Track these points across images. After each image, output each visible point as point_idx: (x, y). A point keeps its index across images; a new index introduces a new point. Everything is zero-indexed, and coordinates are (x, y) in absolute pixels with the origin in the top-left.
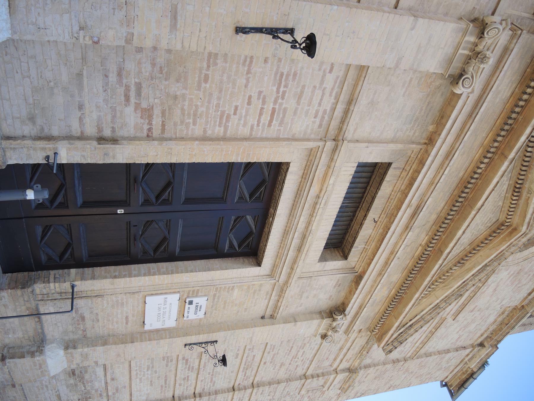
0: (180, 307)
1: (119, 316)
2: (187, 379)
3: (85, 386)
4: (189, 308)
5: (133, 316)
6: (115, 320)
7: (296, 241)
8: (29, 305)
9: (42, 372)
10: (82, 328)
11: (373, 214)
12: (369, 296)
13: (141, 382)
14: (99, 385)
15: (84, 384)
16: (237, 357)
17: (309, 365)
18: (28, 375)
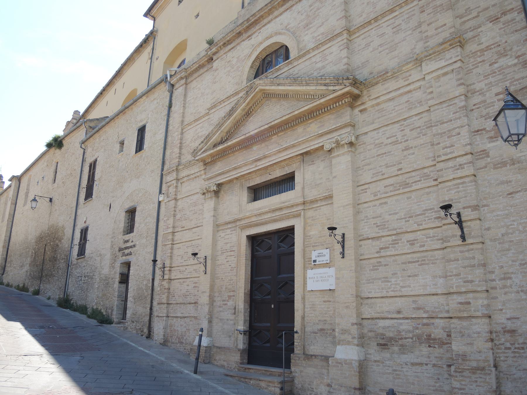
1: (323, 306)
2: (412, 243)
3: (406, 338)
4: (319, 261)
5: (324, 297)
6: (325, 309)
7: (278, 213)
8: (302, 359)
9: (346, 364)
10: (331, 331)
12: (310, 139)
14: (406, 326)
15: (401, 339)
16: (386, 203)
18: (347, 374)
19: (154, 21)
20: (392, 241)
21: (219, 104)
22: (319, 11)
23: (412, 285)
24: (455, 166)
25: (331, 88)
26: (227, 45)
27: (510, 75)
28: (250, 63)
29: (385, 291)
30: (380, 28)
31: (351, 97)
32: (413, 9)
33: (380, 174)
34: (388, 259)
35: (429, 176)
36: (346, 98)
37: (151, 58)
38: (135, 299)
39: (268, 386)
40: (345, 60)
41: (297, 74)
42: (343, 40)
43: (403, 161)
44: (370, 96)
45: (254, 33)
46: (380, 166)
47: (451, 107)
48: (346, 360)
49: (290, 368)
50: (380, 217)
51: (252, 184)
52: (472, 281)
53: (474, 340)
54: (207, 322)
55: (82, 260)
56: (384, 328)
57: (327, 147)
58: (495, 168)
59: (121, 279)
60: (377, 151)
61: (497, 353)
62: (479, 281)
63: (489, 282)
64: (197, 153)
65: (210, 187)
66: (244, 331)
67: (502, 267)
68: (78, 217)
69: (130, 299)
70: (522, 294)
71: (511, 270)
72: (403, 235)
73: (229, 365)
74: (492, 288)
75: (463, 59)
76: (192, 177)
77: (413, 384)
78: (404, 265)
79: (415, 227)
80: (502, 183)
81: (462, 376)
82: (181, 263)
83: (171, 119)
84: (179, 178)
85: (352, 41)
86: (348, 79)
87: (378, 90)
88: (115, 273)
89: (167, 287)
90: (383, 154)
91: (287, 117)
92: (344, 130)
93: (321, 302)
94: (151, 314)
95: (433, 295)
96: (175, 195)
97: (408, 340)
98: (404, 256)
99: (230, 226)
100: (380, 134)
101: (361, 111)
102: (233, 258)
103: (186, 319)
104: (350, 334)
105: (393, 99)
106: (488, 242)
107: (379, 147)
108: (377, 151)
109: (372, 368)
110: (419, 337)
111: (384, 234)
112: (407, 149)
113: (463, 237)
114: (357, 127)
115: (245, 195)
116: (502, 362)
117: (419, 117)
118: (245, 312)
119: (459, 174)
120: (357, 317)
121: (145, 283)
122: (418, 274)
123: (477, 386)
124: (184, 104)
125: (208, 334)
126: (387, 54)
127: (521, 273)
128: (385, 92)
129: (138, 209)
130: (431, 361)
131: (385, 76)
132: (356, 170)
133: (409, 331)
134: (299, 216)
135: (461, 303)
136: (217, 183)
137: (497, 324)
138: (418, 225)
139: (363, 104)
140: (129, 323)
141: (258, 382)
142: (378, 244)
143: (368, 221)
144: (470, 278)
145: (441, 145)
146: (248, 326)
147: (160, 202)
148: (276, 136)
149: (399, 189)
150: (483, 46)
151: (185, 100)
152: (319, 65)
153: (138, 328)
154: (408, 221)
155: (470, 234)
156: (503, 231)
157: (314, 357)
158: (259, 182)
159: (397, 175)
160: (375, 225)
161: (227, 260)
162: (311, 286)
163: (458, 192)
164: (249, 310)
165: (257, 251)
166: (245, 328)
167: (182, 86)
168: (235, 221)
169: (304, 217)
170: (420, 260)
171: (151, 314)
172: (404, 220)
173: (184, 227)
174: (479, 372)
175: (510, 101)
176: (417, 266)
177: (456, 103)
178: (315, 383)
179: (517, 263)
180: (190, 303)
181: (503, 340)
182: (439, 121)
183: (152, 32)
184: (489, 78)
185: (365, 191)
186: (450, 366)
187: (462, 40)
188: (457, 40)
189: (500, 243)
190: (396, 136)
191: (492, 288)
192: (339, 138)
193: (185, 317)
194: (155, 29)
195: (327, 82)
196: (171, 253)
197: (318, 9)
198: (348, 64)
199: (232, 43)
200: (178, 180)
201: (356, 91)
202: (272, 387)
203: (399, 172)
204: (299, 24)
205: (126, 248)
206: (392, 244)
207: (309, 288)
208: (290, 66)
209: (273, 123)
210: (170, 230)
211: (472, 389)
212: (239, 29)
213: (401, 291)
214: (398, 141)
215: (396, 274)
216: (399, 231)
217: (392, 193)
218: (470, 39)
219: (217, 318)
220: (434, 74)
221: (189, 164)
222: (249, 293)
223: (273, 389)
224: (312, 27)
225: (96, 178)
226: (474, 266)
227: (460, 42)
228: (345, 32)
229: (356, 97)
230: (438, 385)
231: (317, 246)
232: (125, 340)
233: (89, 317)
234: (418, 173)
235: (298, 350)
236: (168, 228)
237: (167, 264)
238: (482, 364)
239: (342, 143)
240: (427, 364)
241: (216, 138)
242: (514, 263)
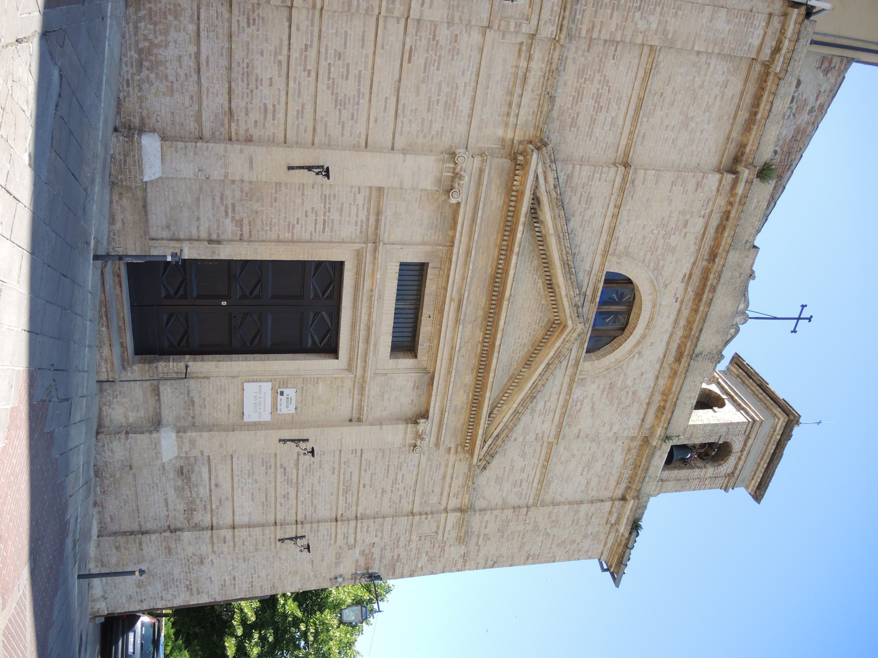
2: (286, 496)
3: (191, 492)
7: (363, 333)
13: (242, 495)
14: (203, 491)
15: (190, 488)
16: (333, 473)
21: (618, 203)
29: (239, 473)
39: (106, 361)
48: (160, 453)
50: (320, 467)
52: (243, 544)
56: (200, 472)
60: (394, 466)
64: (545, 163)
73: (119, 236)
77: (147, 500)
79: (301, 498)
80: (323, 557)
81: (162, 541)
92: (435, 439)
93: (229, 400)
95: (233, 512)
99: (372, 219)
102: (311, 228)
110: (193, 502)
111: (300, 472)
131: (471, 479)
133: (198, 495)
135: (225, 538)
139: (456, 452)
141: (107, 343)
144: (247, 543)
148: (481, 339)
149: (344, 485)
157: (157, 398)
161: (310, 211)
162: (250, 389)
178: (125, 400)
195: (500, 440)
202: (107, 368)
203: (361, 486)
209: (496, 355)
215: (256, 483)
217: (342, 479)
223: (104, 370)
226: (256, 545)
231: (302, 393)
234: (355, 501)
238: (173, 551)
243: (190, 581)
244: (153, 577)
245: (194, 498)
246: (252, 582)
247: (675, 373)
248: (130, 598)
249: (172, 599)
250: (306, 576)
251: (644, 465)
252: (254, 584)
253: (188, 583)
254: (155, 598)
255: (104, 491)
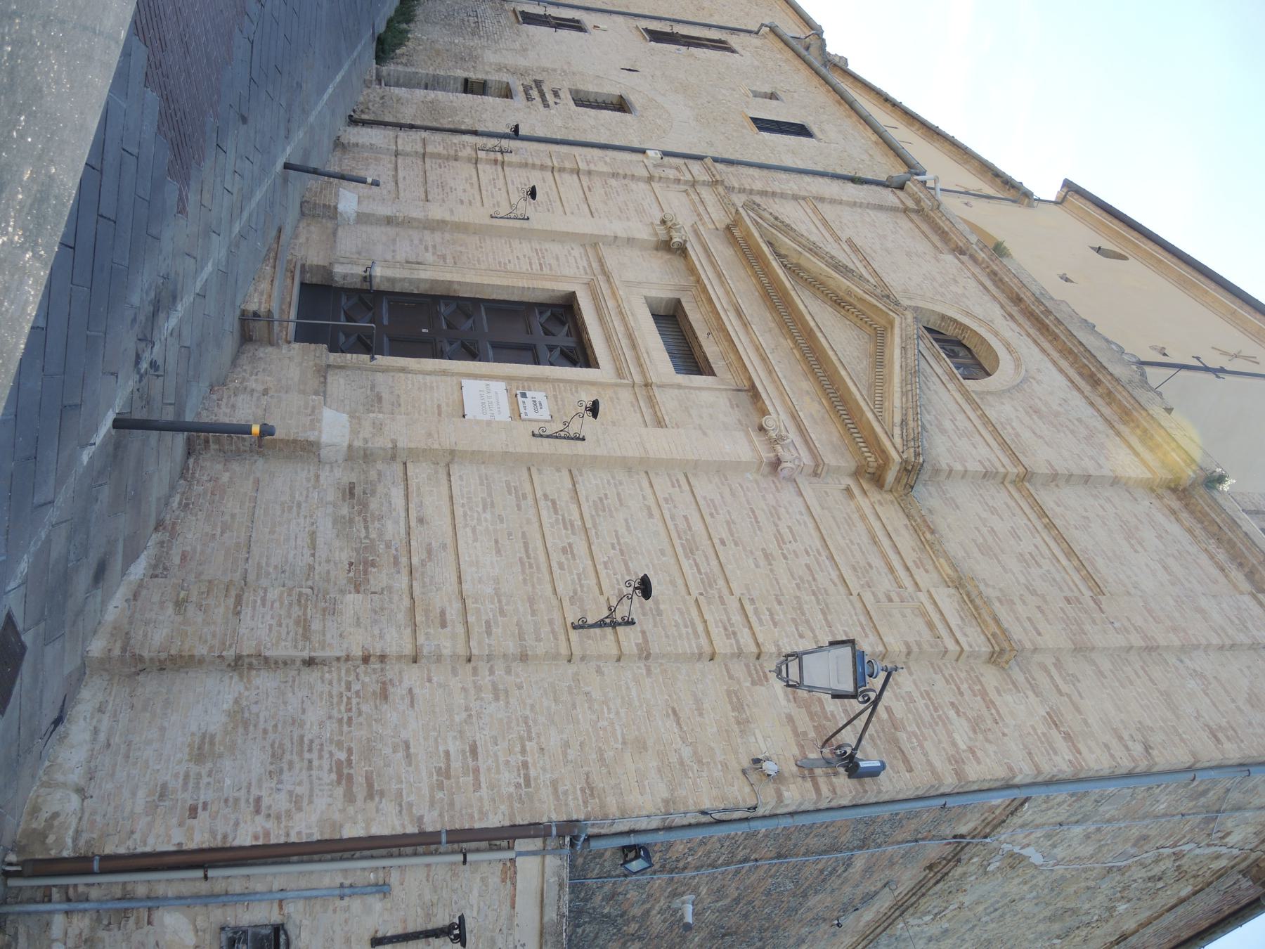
0: (511, 404)
2: (568, 550)
3: (366, 528)
5: (448, 405)
6: (423, 407)
7: (624, 342)
8: (318, 361)
9: (312, 421)
11: (701, 334)
13: (475, 540)
14: (393, 529)
15: (365, 521)
16: (651, 515)
17: (838, 573)
19: (1055, 203)
20: (570, 520)
21: (862, 258)
22: (1068, 432)
23: (478, 545)
24: (732, 625)
25: (897, 431)
26: (992, 280)
27: (932, 734)
28: (951, 313)
29: (465, 501)
30: (1031, 533)
31: (879, 467)
32: (1075, 589)
33: (713, 511)
34: (532, 511)
35: (711, 586)
36: (876, 458)
37: (967, 193)
38: (432, 102)
39: (262, 294)
40: (958, 467)
41: (929, 388)
42: (1004, 466)
43: (741, 548)
44: (881, 504)
45: (1019, 325)
46: (729, 512)
47: (859, 629)
48: (319, 421)
49: (296, 341)
50: (621, 504)
51: (688, 307)
52: (489, 633)
53: (366, 629)
54: (389, 214)
55: (513, 18)
57: (769, 422)
58: (729, 693)
59: (473, 83)
60: (763, 510)
61: (339, 669)
62: (490, 645)
63: (489, 665)
64: (753, 209)
65: (678, 230)
66: (370, 276)
67: (520, 687)
68: (606, 16)
69: (431, 95)
70: (464, 715)
71: (512, 701)
72: (583, 537)
74: (475, 670)
75: (964, 655)
76: (701, 209)
77: (272, 532)
78: (520, 535)
79: (601, 558)
80: (698, 701)
81: (291, 605)
82: (513, 182)
83: (827, 180)
84: (698, 188)
85: (1001, 486)
86: (917, 455)
87: (892, 516)
88: (487, 73)
89: (460, 154)
90: (756, 518)
91: (834, 358)
94: (400, 126)
95: (460, 577)
96: (660, 178)
97: (363, 531)
98: (539, 536)
99: (595, 265)
100: (798, 517)
101: (848, 490)
103: (393, 184)
104: (374, 435)
105: (875, 543)
106: (571, 669)
107: (771, 513)
108: (763, 510)
109: (303, 470)
110: (371, 548)
112: (768, 557)
113: (581, 626)
114: (815, 480)
115: (663, 292)
116: (319, 674)
117: (837, 581)
118: (411, 281)
119: (716, 632)
120: (410, 450)
121: (466, 120)
122: (501, 555)
123: (271, 626)
124: (861, 205)
125: (364, 214)
126: (974, 541)
127: (508, 717)
128: (889, 528)
129: (627, 117)
130: (320, 564)
132: (722, 469)
133: (381, 534)
134: (619, 373)
135: (443, 613)
136: (688, 246)
137: (400, 672)
138: (605, 563)
139: (864, 492)
140: (379, 91)
142: (564, 498)
143: (612, 486)
145: (778, 607)
146: (382, 288)
147: (643, 151)
149: (680, 538)
150: (993, 695)
151: (868, 206)
152: (948, 424)
153: (370, 104)
154: (613, 548)
155: (589, 638)
156: (597, 695)
157: (322, 379)
158: (691, 318)
159: (710, 538)
160: (603, 496)
161: (521, 257)
163: (677, 625)
164: (416, 292)
165: (541, 313)
166: (378, 280)
167: (902, 201)
168: (607, 276)
169: (616, 385)
170: (532, 561)
171: (400, 126)
172: (615, 541)
173: (590, 190)
174: (300, 631)
175: (871, 670)
176: (518, 555)
177: (867, 636)
178: (269, 378)
179: (528, 712)
180: (426, 192)
181: (367, 679)
182: (828, 608)
183: (1027, 195)
184: (924, 699)
185: (675, 484)
186: (312, 588)
187: (1006, 657)
188: (1006, 645)
189: (570, 687)
190: (796, 541)
191: (475, 670)
192: (789, 440)
193: (397, 183)
194: (1035, 203)
196: (534, 166)
197: (1072, 432)
198: (951, 471)
199: (998, 287)
200: (694, 184)
201: (890, 477)
204: (1041, 399)
205: (542, 95)
206: (564, 519)
207: (466, 383)
208: (945, 378)
209: (819, 335)
210: (583, 166)
211: (263, 617)
212: (1029, 298)
213: (466, 526)
214: (785, 543)
216: (592, 533)
217: (671, 527)
218: (1009, 676)
219: (397, 234)
220: (930, 608)
221: (725, 203)
222: (452, 294)
224: (1032, 419)
225: (693, 50)
226: (521, 638)
227: (1002, 651)
228: (1021, 469)
229: (877, 480)
230: (271, 570)
232: (346, 67)
233: (390, 21)
234: (716, 569)
235: (335, 358)
236: (588, 163)
237: (507, 157)
239: (779, 447)
240: (313, 555)
241: (786, 244)
242: (528, 708)
243: (350, 751)
244: (246, 728)
245: (372, 541)
246: (525, 765)
247: (1110, 393)
248: (162, 796)
249: (288, 812)
250: (674, 759)
251: (1223, 520)
252: (532, 773)
253: (343, 756)
254: (237, 800)
255: (187, 505)
